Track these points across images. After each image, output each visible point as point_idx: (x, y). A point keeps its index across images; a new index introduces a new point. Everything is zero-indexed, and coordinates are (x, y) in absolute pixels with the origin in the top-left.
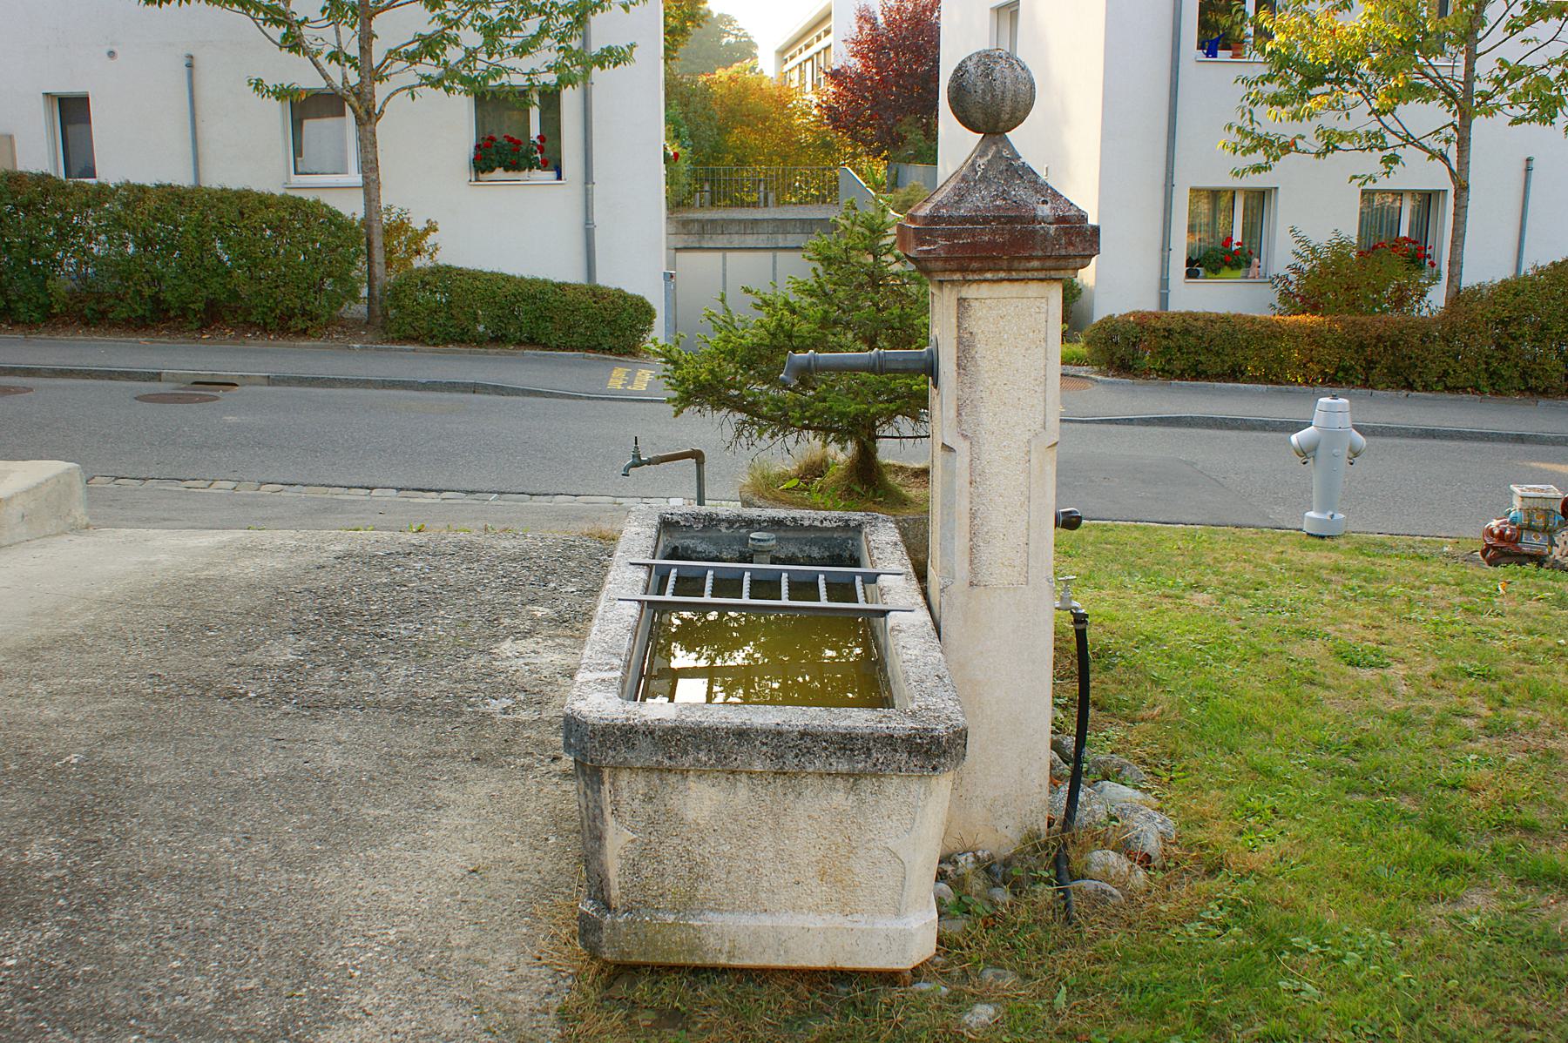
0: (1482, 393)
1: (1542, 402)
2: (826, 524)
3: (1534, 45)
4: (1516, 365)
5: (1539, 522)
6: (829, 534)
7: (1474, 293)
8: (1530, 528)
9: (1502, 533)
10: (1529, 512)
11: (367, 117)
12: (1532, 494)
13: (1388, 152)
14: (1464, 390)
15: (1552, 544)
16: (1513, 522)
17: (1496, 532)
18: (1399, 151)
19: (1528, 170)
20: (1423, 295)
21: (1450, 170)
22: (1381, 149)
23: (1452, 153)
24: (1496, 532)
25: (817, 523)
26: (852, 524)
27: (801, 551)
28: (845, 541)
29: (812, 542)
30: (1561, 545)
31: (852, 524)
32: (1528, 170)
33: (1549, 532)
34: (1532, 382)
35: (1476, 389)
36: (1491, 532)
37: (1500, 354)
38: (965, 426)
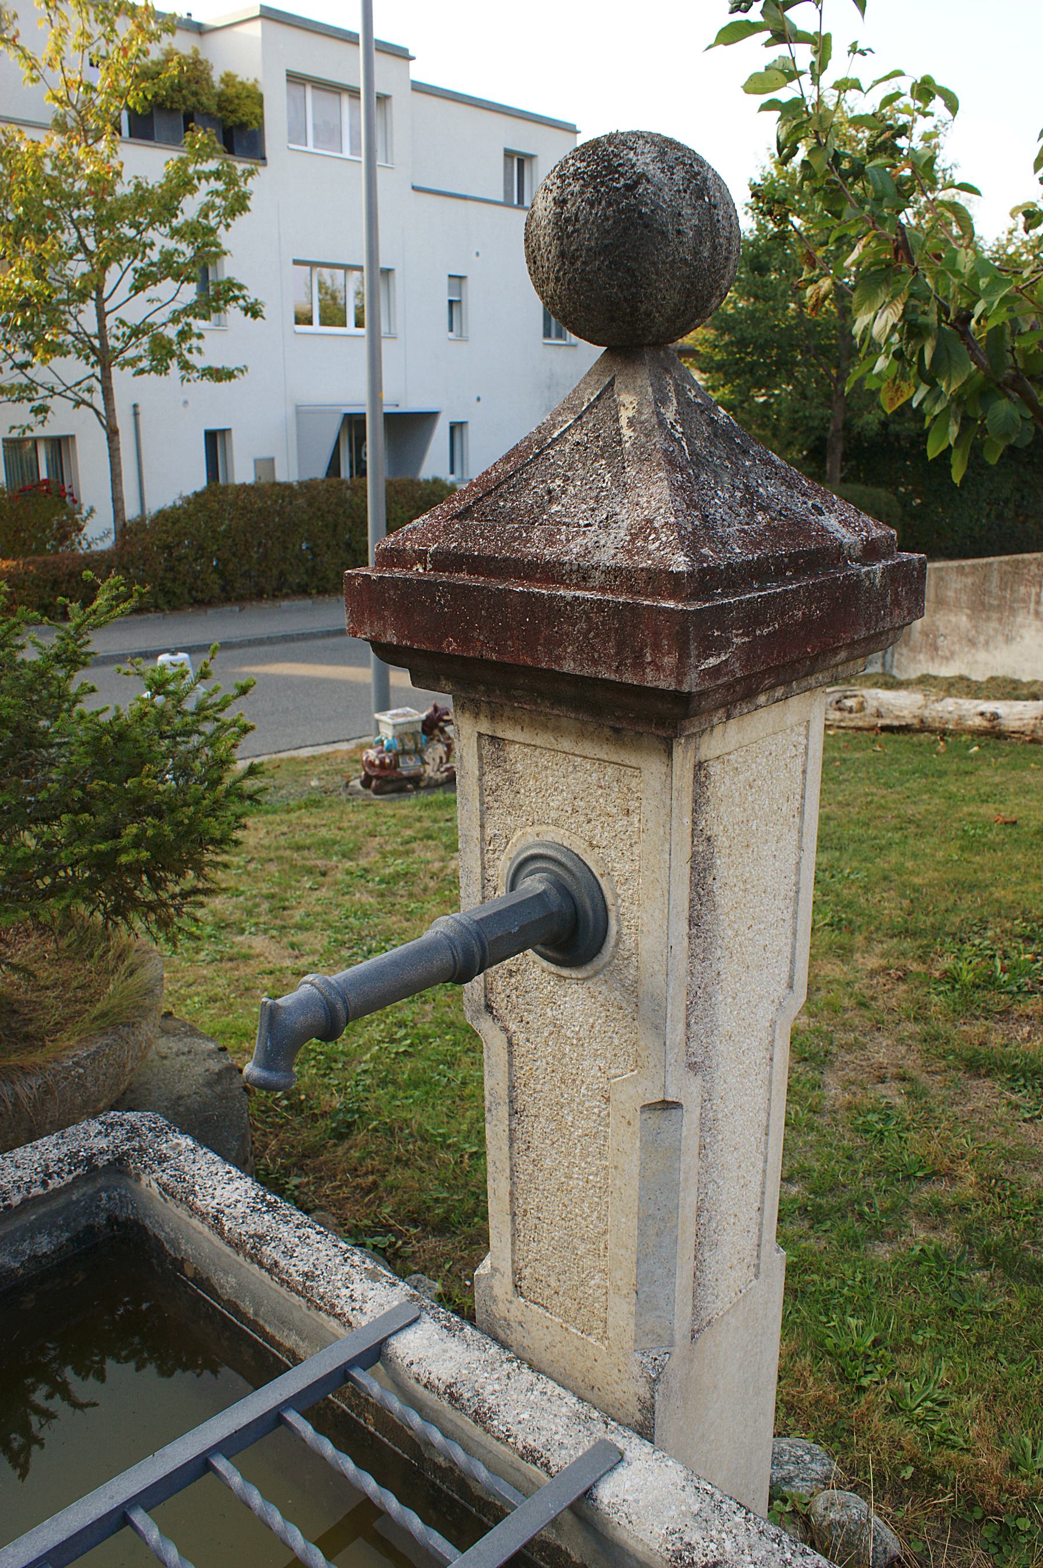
0: (162, 610)
1: (210, 611)
2: (54, 1183)
3: (157, 305)
4: (184, 583)
5: (410, 745)
6: (62, 1201)
7: (140, 525)
8: (405, 752)
9: (382, 762)
10: (400, 737)
11: (507, 204)
12: (401, 720)
13: (36, 403)
14: (148, 611)
15: (424, 763)
16: (389, 750)
17: (377, 762)
18: (49, 402)
19: (136, 414)
20: (80, 529)
21: (98, 413)
22: (30, 400)
23: (100, 405)
24: (377, 762)
25: (37, 1190)
26: (101, 1162)
27: (15, 1255)
28: (95, 1198)
29: (32, 1231)
30: (431, 762)
31: (101, 1162)
32: (136, 414)
33: (419, 752)
34: (200, 596)
35: (157, 608)
36: (371, 764)
37: (170, 575)
38: (694, 1045)
